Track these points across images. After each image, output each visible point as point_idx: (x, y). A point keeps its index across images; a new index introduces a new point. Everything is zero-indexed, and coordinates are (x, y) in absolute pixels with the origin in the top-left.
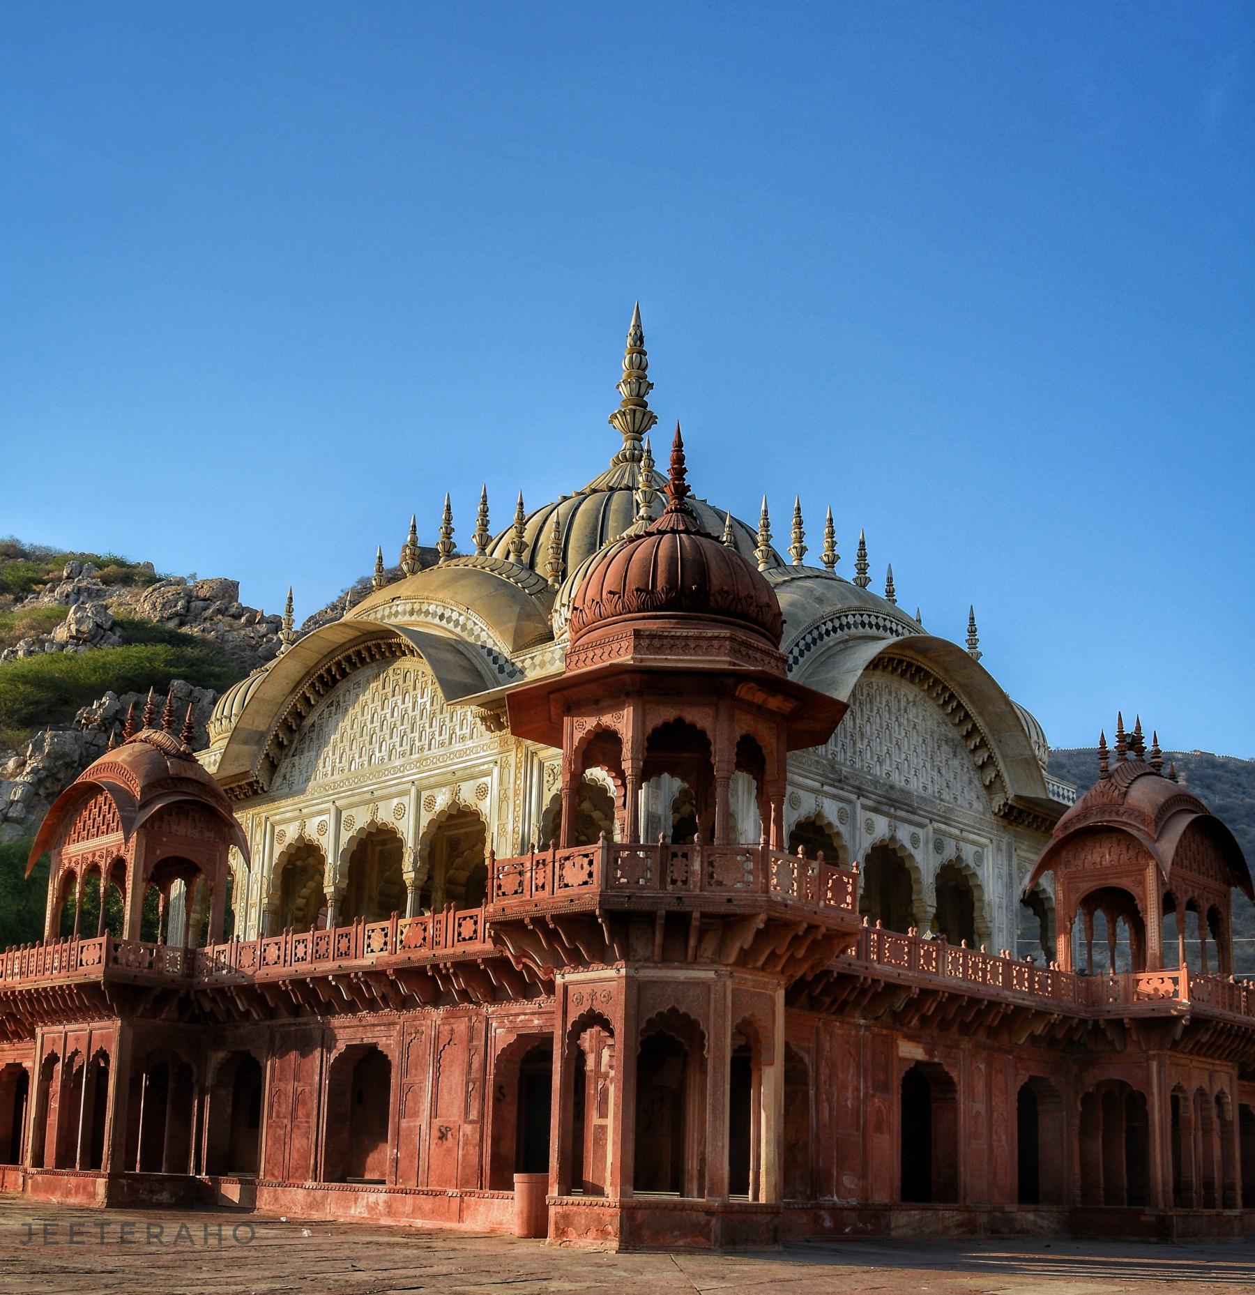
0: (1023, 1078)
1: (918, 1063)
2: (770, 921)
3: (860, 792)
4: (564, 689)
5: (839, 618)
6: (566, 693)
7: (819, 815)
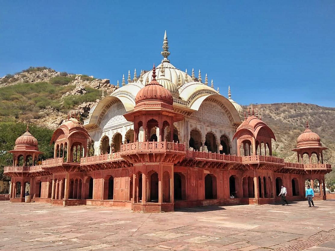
1: (208, 174)
4: (134, 114)
5: (199, 92)
6: (134, 114)
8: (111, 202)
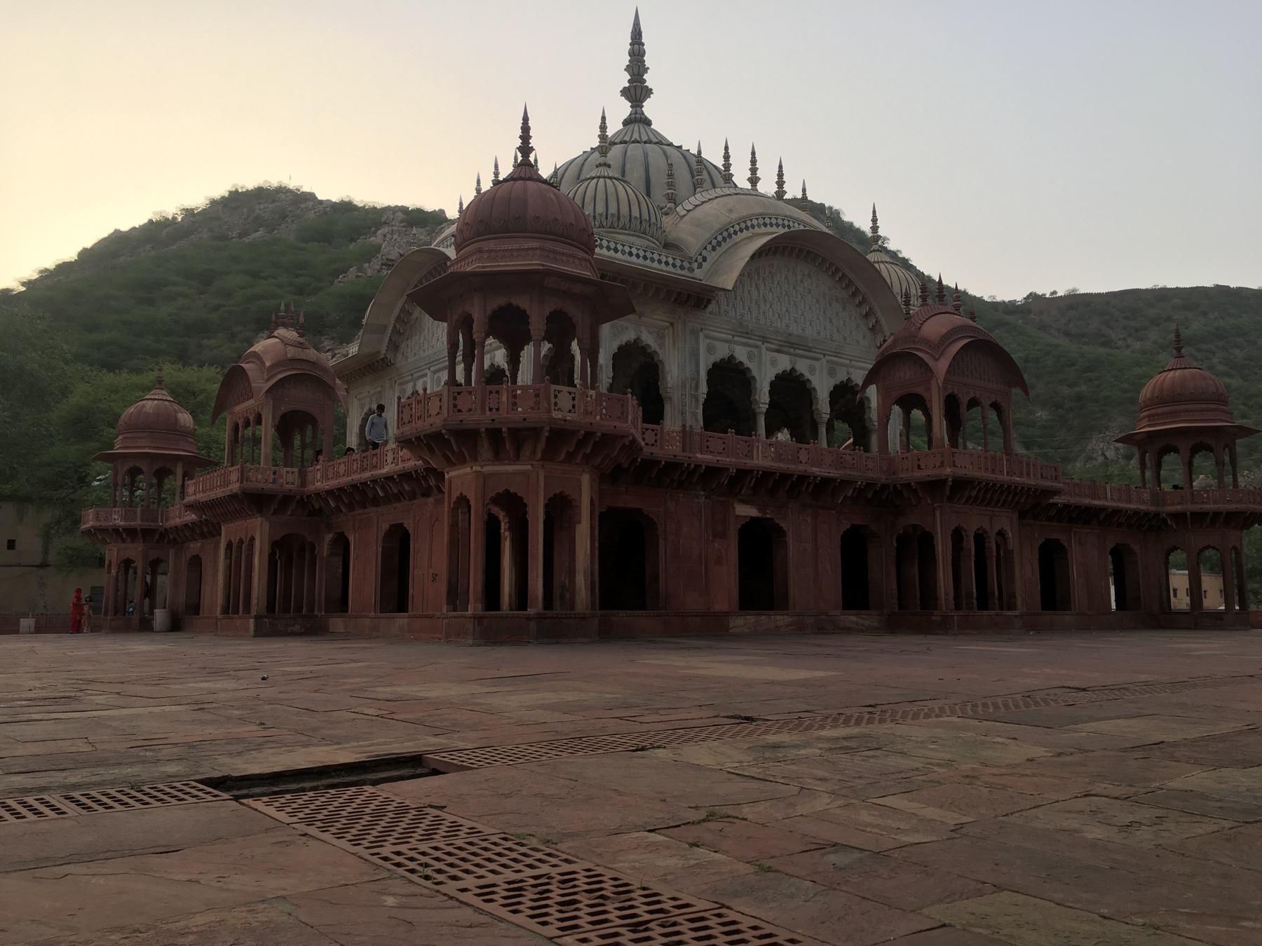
0: (846, 526)
2: (551, 431)
3: (764, 339)
7: (732, 357)
8: (401, 620)
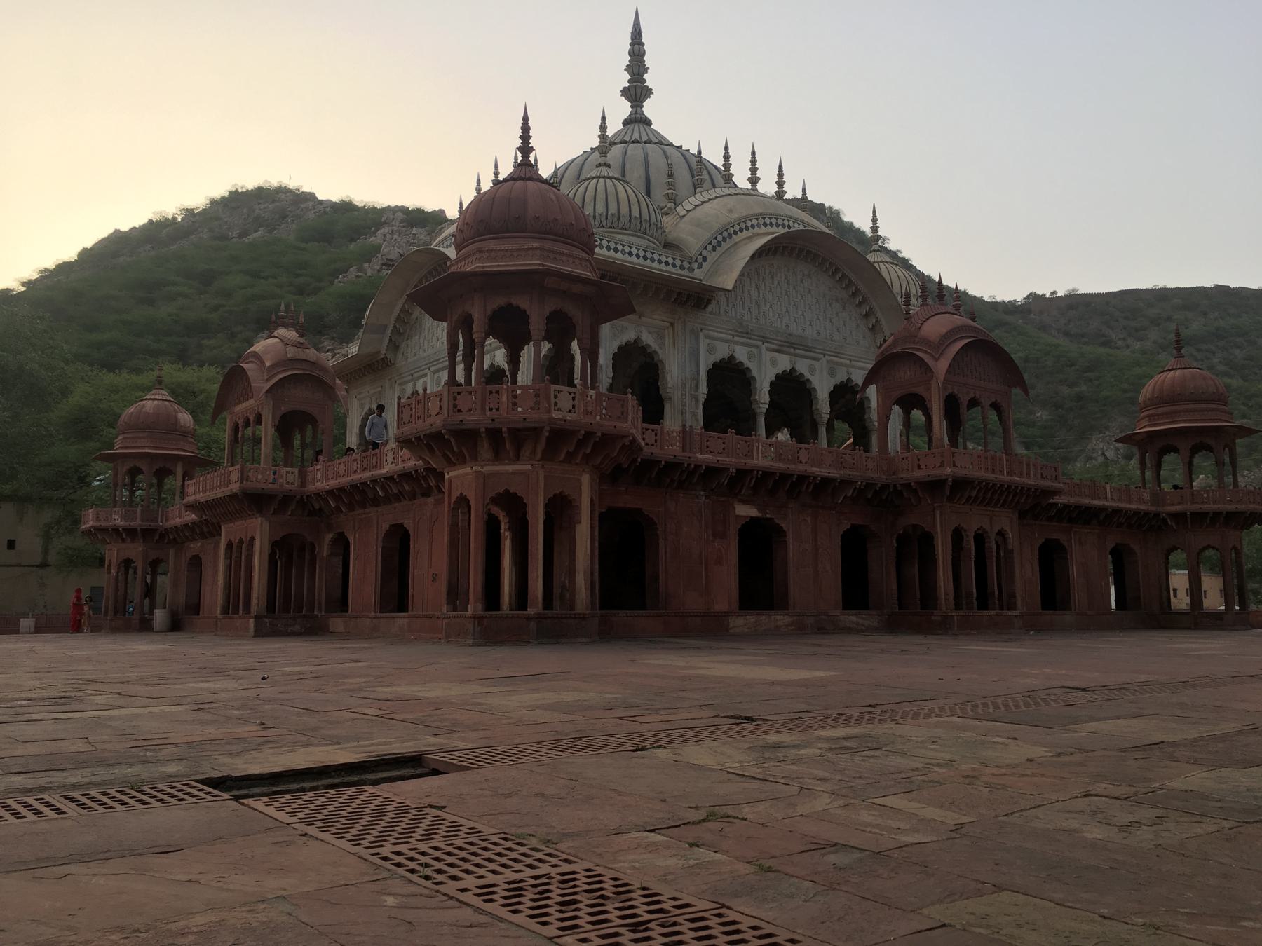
0: (846, 526)
2: (551, 431)
3: (764, 339)
7: (732, 357)
8: (401, 620)
